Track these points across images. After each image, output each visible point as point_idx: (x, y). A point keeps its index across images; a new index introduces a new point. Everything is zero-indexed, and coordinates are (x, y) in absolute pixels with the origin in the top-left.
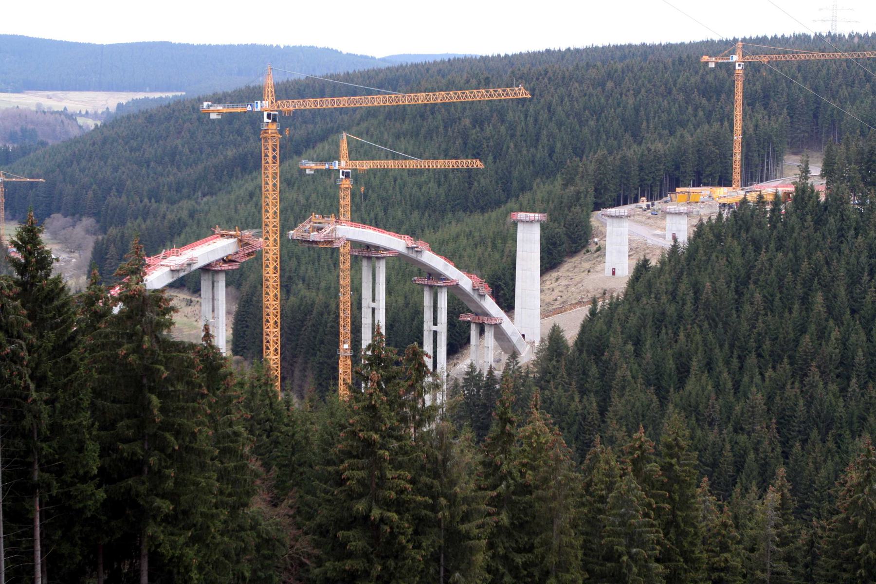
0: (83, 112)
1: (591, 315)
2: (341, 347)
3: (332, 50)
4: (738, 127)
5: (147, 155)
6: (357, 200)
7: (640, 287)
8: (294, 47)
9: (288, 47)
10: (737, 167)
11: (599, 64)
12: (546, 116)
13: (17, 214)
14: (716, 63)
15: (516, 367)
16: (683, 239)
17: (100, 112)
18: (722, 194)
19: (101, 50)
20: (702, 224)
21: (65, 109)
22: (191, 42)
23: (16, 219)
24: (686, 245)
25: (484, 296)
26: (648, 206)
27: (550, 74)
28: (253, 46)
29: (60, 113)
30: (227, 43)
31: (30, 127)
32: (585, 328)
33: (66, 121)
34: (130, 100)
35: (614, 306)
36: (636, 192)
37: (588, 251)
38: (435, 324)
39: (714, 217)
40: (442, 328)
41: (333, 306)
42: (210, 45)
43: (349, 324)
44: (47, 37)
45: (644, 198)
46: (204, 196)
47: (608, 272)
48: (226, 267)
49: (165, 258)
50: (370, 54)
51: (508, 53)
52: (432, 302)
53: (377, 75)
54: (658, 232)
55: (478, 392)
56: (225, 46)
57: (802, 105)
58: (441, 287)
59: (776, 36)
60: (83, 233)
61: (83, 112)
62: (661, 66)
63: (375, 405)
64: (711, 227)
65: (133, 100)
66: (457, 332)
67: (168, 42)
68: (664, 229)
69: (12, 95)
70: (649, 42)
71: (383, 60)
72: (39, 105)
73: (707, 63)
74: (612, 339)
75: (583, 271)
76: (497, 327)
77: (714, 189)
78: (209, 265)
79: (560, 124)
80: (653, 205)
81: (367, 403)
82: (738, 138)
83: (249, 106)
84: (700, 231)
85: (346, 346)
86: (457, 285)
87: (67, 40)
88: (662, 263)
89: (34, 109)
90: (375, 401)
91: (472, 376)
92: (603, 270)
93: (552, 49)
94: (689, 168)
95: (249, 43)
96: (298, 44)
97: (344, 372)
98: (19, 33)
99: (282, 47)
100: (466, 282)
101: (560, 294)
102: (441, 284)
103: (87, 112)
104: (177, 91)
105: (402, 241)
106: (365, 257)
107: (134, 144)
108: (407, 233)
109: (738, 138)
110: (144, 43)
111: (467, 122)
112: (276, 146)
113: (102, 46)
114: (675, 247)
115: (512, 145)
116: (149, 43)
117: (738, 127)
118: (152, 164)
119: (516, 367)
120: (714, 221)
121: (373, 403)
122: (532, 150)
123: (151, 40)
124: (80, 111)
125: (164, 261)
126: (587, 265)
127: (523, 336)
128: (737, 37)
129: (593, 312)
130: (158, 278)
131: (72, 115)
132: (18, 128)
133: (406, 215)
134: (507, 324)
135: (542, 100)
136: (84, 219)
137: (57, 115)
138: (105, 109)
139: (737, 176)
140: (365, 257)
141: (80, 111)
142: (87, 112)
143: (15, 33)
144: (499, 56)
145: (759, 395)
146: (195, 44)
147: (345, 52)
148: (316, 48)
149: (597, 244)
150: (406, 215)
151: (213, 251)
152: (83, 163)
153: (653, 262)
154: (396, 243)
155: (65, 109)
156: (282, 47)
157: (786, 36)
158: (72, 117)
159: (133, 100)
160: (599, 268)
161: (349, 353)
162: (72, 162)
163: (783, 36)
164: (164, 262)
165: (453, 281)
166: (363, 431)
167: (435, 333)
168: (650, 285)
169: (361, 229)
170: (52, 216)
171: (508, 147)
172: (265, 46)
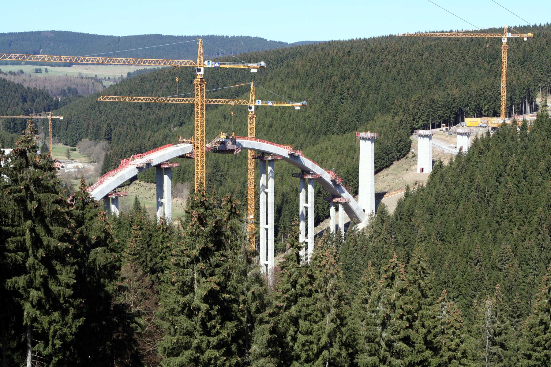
0: (107, 78)
1: (405, 196)
4: (504, 79)
6: (261, 125)
7: (437, 179)
8: (237, 37)
9: (234, 37)
11: (420, 42)
13: (62, 139)
14: (528, 38)
16: (465, 149)
17: (117, 78)
18: (496, 122)
20: (477, 139)
21: (96, 76)
23: (61, 142)
24: (467, 153)
26: (447, 129)
27: (389, 48)
29: (92, 78)
31: (73, 87)
32: (400, 204)
33: (95, 84)
34: (135, 70)
35: (421, 190)
36: (440, 121)
37: (407, 158)
39: (485, 136)
41: (245, 193)
45: (444, 124)
46: (175, 127)
47: (419, 171)
49: (133, 159)
50: (284, 41)
51: (366, 38)
54: (453, 145)
57: (548, 66)
59: (535, 25)
60: (100, 150)
61: (107, 78)
64: (482, 140)
65: (137, 70)
68: (456, 143)
72: (80, 74)
74: (416, 211)
75: (404, 170)
77: (490, 119)
80: (450, 128)
82: (503, 85)
84: (475, 143)
85: (252, 217)
86: (321, 177)
87: (98, 34)
88: (451, 163)
89: (76, 75)
92: (416, 169)
93: (393, 34)
96: (240, 35)
98: (69, 30)
100: (328, 177)
101: (388, 184)
103: (109, 78)
105: (285, 150)
108: (287, 144)
109: (503, 85)
110: (145, 35)
114: (460, 153)
116: (148, 35)
117: (504, 79)
120: (484, 137)
122: (376, 95)
123: (149, 33)
124: (105, 78)
125: (133, 161)
126: (406, 166)
127: (364, 210)
128: (511, 26)
129: (407, 195)
131: (100, 79)
132: (66, 88)
134: (353, 203)
135: (383, 64)
136: (101, 142)
137: (90, 80)
138: (120, 76)
139: (503, 110)
141: (105, 78)
142: (109, 78)
143: (66, 30)
144: (360, 39)
145: (509, 246)
146: (176, 36)
147: (268, 39)
148: (251, 37)
149: (413, 153)
151: (163, 155)
153: (446, 163)
154: (284, 151)
155: (96, 76)
157: (542, 25)
158: (99, 81)
159: (137, 70)
160: (413, 168)
163: (540, 25)
164: (132, 162)
165: (317, 175)
166: (187, 250)
168: (442, 177)
169: (258, 142)
172: (219, 37)
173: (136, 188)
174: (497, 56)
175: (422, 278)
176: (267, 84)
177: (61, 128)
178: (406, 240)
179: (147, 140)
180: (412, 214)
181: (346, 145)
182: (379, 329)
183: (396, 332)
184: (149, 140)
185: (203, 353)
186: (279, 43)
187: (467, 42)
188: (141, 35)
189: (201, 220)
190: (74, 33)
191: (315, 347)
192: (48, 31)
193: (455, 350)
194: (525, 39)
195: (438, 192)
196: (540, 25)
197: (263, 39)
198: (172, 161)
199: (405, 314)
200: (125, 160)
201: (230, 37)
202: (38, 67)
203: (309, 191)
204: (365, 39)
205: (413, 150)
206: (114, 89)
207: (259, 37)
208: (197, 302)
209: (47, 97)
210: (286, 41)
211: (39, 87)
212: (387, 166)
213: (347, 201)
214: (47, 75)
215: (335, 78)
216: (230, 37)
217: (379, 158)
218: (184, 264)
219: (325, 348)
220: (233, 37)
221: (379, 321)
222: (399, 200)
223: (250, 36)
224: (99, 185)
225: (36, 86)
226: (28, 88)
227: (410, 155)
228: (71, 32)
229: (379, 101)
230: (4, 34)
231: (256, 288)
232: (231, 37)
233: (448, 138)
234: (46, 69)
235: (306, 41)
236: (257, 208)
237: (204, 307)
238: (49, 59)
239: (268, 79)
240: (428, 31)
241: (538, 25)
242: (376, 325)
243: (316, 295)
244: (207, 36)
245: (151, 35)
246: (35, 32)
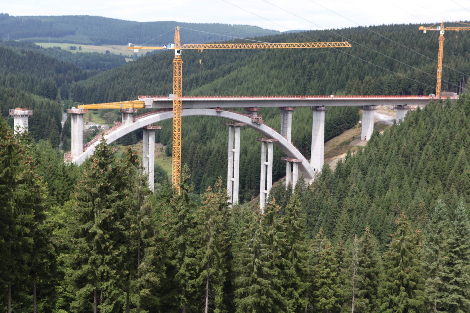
0: (130, 56)
3: (258, 27)
5: (151, 77)
9: (236, 25)
10: (439, 86)
12: (346, 59)
14: (427, 31)
19: (141, 24)
21: (121, 54)
22: (186, 22)
28: (218, 25)
30: (204, 22)
38: (267, 161)
40: (270, 163)
42: (196, 24)
44: (114, 18)
48: (154, 128)
53: (270, 38)
56: (203, 24)
58: (270, 143)
62: (411, 34)
69: (94, 46)
73: (423, 31)
76: (300, 165)
78: (146, 127)
79: (353, 63)
83: (165, 46)
94: (415, 87)
99: (232, 25)
102: (270, 141)
106: (230, 126)
107: (146, 71)
111: (305, 61)
112: (180, 67)
115: (327, 73)
116: (165, 22)
118: (153, 81)
122: (338, 76)
127: (315, 169)
130: (119, 132)
140: (230, 126)
142: (132, 56)
147: (264, 28)
152: (120, 80)
155: (121, 54)
156: (232, 25)
162: (114, 80)
165: (276, 140)
167: (267, 166)
171: (325, 75)
172: (223, 25)
174: (435, 48)
175: (295, 219)
177: (86, 96)
178: (341, 195)
180: (348, 173)
182: (253, 255)
183: (266, 259)
185: (97, 267)
187: (419, 34)
188: (159, 22)
189: (102, 165)
190: (104, 18)
191: (197, 268)
193: (325, 278)
194: (425, 32)
195: (371, 156)
197: (260, 28)
198: (153, 125)
199: (279, 246)
202: (73, 45)
204: (338, 30)
205: (360, 122)
206: (131, 65)
207: (257, 26)
208: (94, 228)
209: (77, 70)
210: (279, 30)
212: (338, 135)
213: (300, 161)
214: (79, 51)
215: (305, 61)
217: (332, 128)
218: (86, 199)
219: (205, 268)
221: (252, 249)
222: (339, 162)
226: (62, 62)
227: (357, 126)
228: (102, 17)
229: (339, 82)
230: (5, 17)
231: (145, 219)
233: (391, 113)
234: (80, 47)
237: (100, 232)
238: (323, 46)
242: (250, 252)
243: (199, 227)
245: (168, 22)
246: (72, 16)
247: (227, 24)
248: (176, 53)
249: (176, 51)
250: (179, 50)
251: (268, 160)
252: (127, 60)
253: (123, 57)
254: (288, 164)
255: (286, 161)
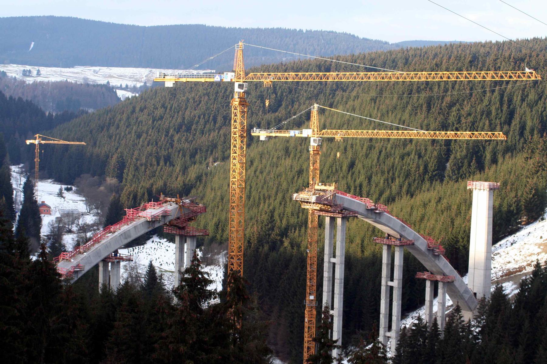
0: (124, 86)
2: (307, 299)
9: (311, 31)
15: (459, 321)
19: (144, 29)
21: (108, 83)
25: (438, 256)
38: (392, 280)
43: (315, 278)
46: (215, 162)
49: (145, 209)
50: (384, 40)
52: (390, 259)
55: (424, 342)
61: (124, 86)
63: (184, 321)
66: (417, 289)
67: (202, 25)
70: (55, 15)
71: (397, 45)
81: (178, 318)
85: (312, 297)
90: (185, 317)
91: (419, 328)
95: (211, 26)
96: (319, 29)
97: (309, 321)
103: (127, 86)
104: (208, 68)
113: (144, 28)
119: (459, 321)
121: (183, 318)
124: (121, 85)
133: (388, 183)
141: (121, 85)
142: (127, 86)
144: (491, 42)
146: (227, 27)
147: (361, 37)
148: (336, 33)
150: (388, 183)
152: (112, 129)
161: (314, 304)
162: (103, 129)
170: (82, 175)
173: (153, 248)
176: (350, 103)
179: (174, 179)
181: (457, 199)
184: (176, 179)
186: (376, 41)
190: (80, 19)
192: (44, 17)
196: (346, 33)
197: (353, 36)
200: (131, 210)
201: (304, 31)
202: (28, 68)
203: (334, 329)
207: (348, 32)
211: (27, 96)
214: (39, 79)
216: (304, 31)
220: (309, 32)
223: (334, 31)
224: (93, 245)
225: (23, 95)
232: (307, 31)
234: (39, 71)
235: (416, 41)
236: (320, 286)
239: (352, 98)
240: (488, 40)
241: (345, 32)
244: (271, 29)
247: (301, 31)
248: (237, 89)
249: (236, 85)
250: (241, 83)
251: (335, 306)
252: (121, 94)
253: (113, 87)
254: (428, 284)
255: (425, 280)
